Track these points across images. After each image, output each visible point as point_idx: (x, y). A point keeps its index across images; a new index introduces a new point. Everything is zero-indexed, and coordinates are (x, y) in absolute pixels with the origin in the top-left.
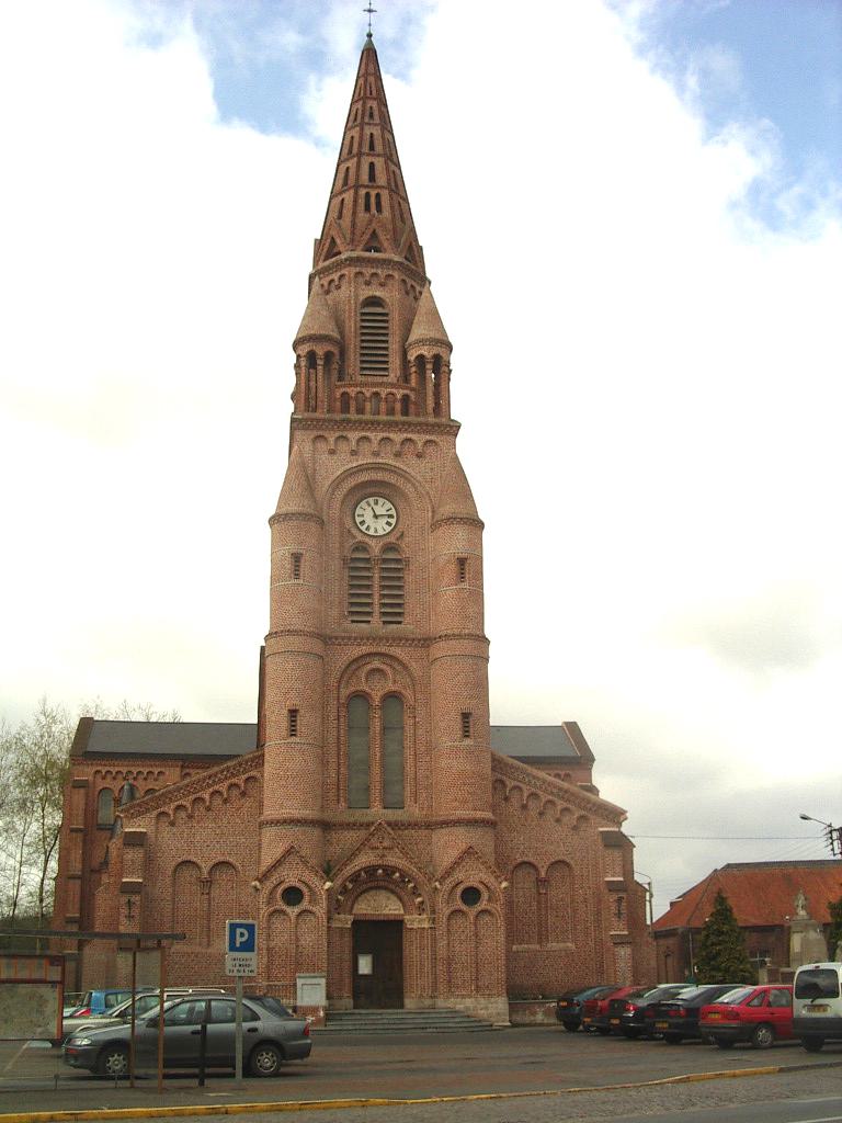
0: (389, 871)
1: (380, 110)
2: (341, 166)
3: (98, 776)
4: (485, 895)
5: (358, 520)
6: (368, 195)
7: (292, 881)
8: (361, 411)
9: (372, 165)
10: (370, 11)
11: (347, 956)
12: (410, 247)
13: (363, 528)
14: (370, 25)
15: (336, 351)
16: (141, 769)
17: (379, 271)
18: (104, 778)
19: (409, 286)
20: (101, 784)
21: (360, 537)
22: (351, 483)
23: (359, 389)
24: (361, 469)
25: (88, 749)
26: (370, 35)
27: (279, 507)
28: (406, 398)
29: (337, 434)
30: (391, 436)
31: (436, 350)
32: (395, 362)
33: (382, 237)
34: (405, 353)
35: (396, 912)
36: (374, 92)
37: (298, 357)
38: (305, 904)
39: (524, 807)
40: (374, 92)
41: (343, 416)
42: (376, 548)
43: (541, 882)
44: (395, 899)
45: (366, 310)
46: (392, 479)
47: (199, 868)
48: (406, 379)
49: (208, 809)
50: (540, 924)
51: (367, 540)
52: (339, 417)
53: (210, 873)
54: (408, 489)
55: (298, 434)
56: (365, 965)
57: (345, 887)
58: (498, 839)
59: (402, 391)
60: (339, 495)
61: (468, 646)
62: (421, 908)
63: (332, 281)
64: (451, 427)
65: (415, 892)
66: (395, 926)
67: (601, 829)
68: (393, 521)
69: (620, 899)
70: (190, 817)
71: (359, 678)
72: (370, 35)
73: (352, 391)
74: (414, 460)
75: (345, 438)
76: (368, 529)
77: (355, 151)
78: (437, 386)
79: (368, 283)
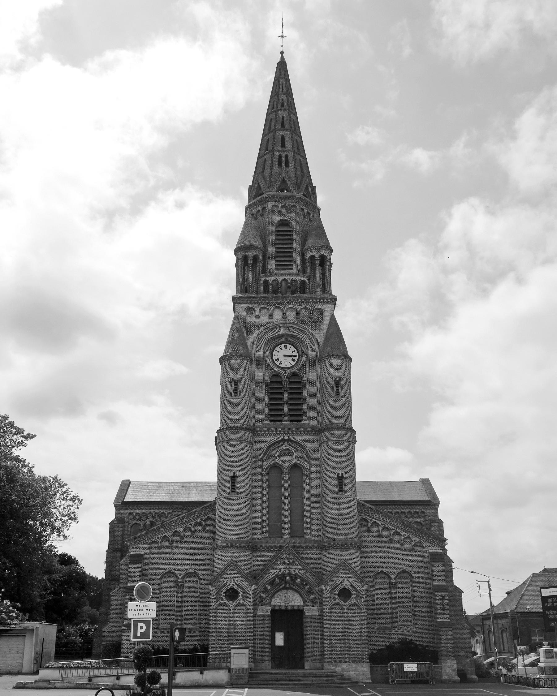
0: (294, 577)
1: (288, 100)
2: (264, 138)
4: (354, 594)
5: (275, 358)
6: (280, 156)
7: (232, 585)
8: (275, 291)
9: (283, 138)
10: (282, 37)
11: (267, 633)
12: (307, 188)
13: (278, 363)
14: (282, 46)
15: (260, 255)
16: (158, 512)
17: (287, 204)
18: (134, 517)
19: (306, 212)
20: (132, 521)
21: (275, 369)
22: (270, 335)
23: (274, 278)
24: (276, 326)
25: (126, 499)
26: (282, 53)
27: (225, 352)
28: (303, 283)
29: (261, 306)
30: (295, 306)
31: (322, 252)
32: (297, 260)
33: (288, 183)
34: (303, 255)
35: (299, 604)
36: (285, 90)
37: (238, 259)
38: (239, 600)
39: (380, 536)
40: (285, 90)
41: (264, 295)
42: (285, 375)
43: (392, 586)
44: (298, 595)
45: (281, 229)
46: (295, 333)
47: (176, 576)
48: (304, 272)
49: (182, 538)
50: (392, 613)
51: (280, 370)
52: (261, 295)
53: (183, 579)
54: (305, 339)
55: (238, 306)
56: (279, 639)
57: (266, 588)
58: (363, 556)
59: (300, 278)
60: (263, 343)
61: (344, 434)
62: (314, 603)
63: (259, 211)
64: (331, 299)
65: (310, 592)
66: (299, 613)
67: (430, 551)
68: (296, 358)
69: (443, 598)
70: (171, 543)
71: (275, 456)
72: (282, 53)
73: (270, 280)
74: (308, 321)
75: (265, 308)
77: (272, 128)
78: (323, 274)
79: (280, 212)
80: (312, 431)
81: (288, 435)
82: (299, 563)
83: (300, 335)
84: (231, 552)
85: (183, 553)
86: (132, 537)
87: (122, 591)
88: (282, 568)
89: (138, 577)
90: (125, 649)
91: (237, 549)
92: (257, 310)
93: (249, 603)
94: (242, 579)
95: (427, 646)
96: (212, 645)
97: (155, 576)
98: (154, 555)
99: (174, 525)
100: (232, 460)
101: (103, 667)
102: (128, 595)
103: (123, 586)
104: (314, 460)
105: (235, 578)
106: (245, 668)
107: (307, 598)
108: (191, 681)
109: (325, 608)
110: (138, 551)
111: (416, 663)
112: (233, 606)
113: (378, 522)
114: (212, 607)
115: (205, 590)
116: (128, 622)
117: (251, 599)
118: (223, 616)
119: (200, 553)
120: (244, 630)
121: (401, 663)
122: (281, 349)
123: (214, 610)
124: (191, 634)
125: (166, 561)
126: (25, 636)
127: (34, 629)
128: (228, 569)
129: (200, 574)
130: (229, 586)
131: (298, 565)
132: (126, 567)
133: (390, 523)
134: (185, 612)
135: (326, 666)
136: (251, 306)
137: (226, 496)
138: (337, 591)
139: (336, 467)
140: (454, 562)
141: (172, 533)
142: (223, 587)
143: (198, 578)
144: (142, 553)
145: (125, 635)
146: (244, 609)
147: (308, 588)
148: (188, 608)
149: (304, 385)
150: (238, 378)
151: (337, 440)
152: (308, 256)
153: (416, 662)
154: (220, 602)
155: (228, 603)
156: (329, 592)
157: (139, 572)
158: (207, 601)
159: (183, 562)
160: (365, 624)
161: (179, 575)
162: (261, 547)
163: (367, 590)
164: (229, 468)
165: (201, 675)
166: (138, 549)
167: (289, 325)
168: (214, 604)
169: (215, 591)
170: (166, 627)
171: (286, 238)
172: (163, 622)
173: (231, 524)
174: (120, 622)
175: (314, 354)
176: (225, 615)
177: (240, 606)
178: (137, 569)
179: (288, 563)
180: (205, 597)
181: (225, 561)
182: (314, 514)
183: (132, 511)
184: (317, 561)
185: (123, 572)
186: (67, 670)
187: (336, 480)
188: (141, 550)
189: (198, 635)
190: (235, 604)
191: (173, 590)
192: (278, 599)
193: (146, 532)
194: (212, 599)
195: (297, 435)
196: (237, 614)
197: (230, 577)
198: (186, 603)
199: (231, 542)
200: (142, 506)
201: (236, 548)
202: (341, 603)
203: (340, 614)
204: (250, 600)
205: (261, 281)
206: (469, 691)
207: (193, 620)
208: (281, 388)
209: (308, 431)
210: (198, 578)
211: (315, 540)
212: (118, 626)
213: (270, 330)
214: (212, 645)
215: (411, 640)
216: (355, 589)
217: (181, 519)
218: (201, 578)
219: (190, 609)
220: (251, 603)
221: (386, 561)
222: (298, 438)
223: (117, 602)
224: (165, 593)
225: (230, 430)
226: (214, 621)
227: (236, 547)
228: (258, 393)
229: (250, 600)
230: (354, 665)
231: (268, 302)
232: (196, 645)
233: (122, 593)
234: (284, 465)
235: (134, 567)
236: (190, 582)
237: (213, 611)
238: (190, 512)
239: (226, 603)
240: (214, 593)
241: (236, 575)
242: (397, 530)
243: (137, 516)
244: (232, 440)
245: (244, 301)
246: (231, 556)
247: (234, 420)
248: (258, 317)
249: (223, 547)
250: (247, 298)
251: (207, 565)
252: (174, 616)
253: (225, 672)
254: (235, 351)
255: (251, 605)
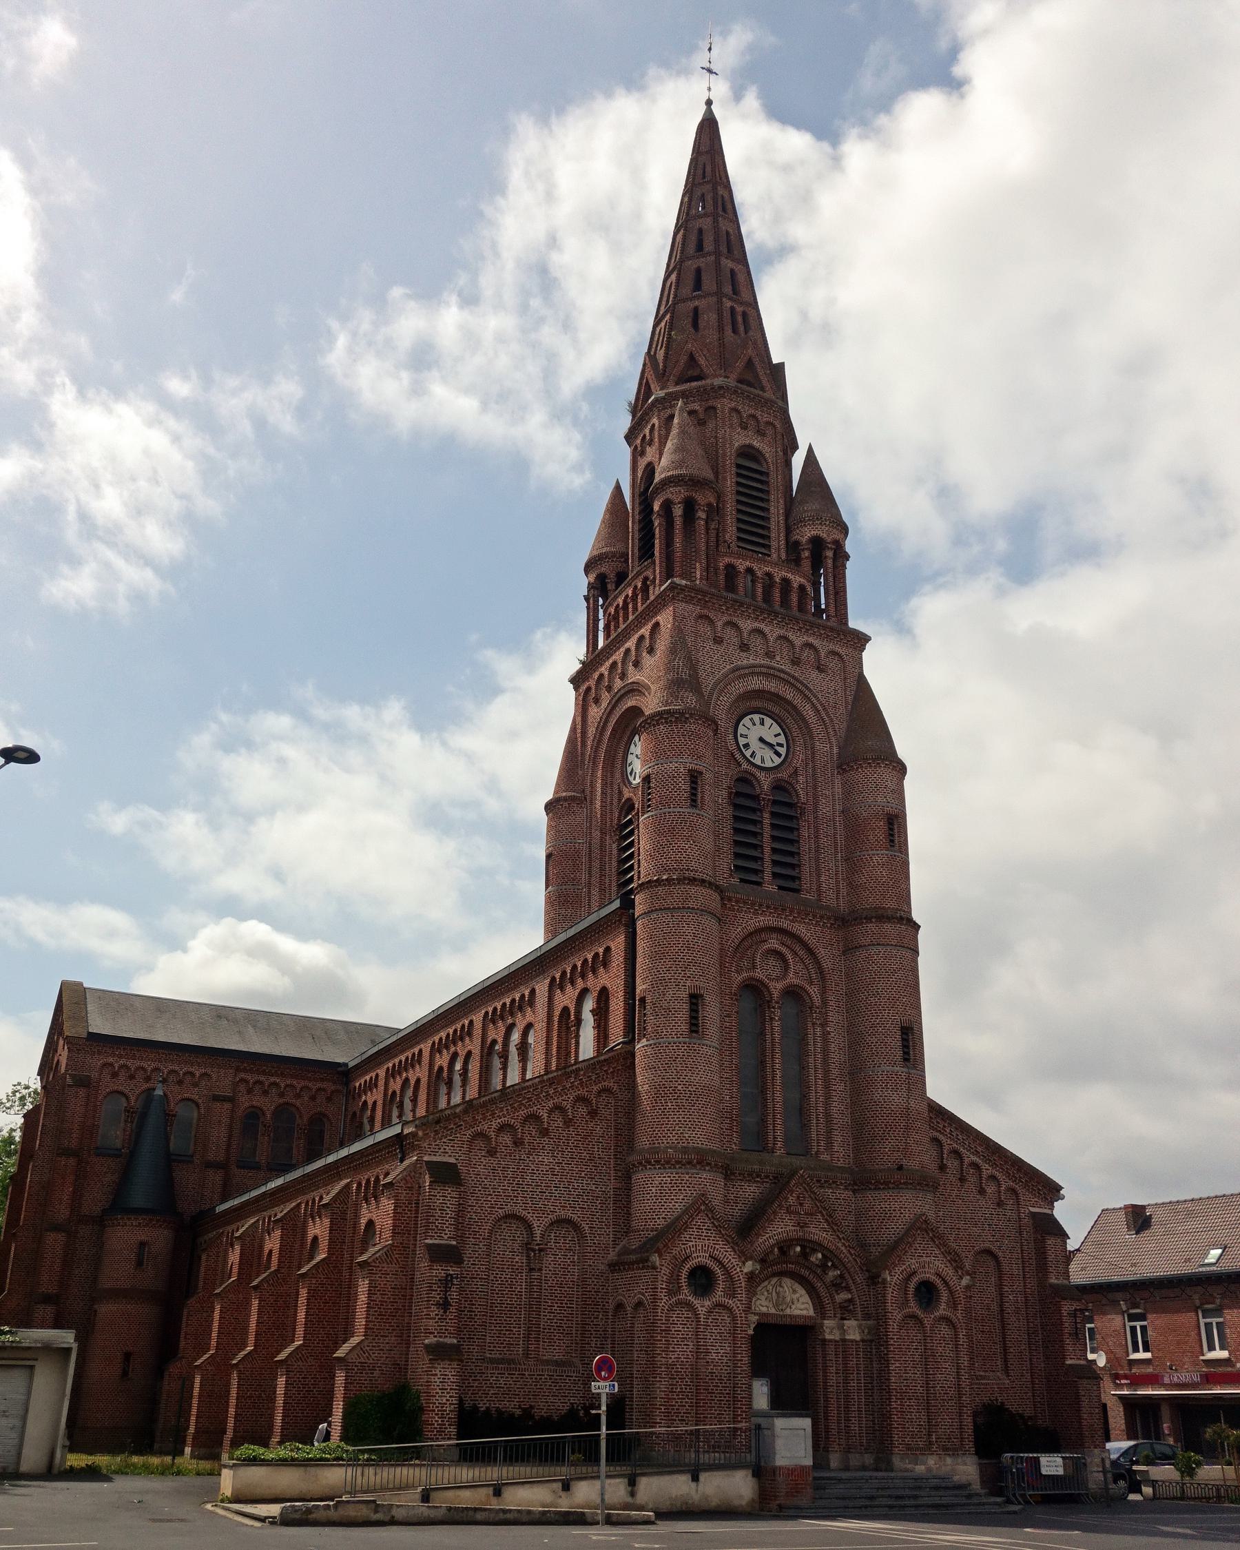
3: (106, 1071)
5: (742, 741)
7: (701, 1258)
10: (710, 71)
13: (748, 754)
18: (115, 1075)
21: (745, 766)
24: (753, 671)
35: (804, 1313)
42: (766, 782)
46: (789, 694)
47: (529, 1227)
49: (545, 1132)
51: (754, 770)
53: (543, 1236)
61: (909, 954)
70: (518, 1143)
72: (709, 103)
74: (814, 674)
76: (753, 754)
80: (829, 918)
81: (782, 918)
82: (823, 1215)
83: (798, 701)
84: (696, 1178)
85: (545, 1170)
86: (431, 1117)
87: (397, 1256)
88: (791, 1224)
89: (452, 1223)
90: (436, 1412)
91: (709, 1170)
92: (719, 624)
93: (739, 1305)
94: (723, 1245)
95: (1030, 1418)
96: (660, 1405)
97: (480, 1224)
98: (476, 1170)
99: (528, 1098)
100: (694, 957)
101: (368, 1460)
102: (435, 1268)
103: (401, 1243)
104: (833, 984)
105: (708, 1240)
106: (806, 1466)
107: (828, 1300)
108: (670, 1498)
109: (890, 1325)
110: (442, 1154)
111: (1060, 1455)
112: (704, 1309)
113: (941, 1137)
114: (659, 1311)
115: (596, 1268)
116: (436, 1339)
117: (742, 1294)
118: (682, 1334)
119: (583, 1175)
120: (726, 1370)
121: (1035, 1455)
122: (754, 724)
123: (664, 1318)
124: (563, 1376)
125: (506, 1188)
126: (32, 1367)
127: (72, 1348)
128: (694, 1218)
129: (583, 1225)
130: (697, 1261)
131: (821, 1220)
132: (408, 1194)
133: (963, 1142)
134: (546, 1320)
135: (897, 1462)
136: (705, 612)
137: (681, 1039)
138: (912, 1285)
139: (898, 1004)
140: (1069, 1238)
141: (522, 1116)
142: (683, 1262)
143: (575, 1236)
144: (452, 1160)
145: (436, 1375)
146: (726, 1318)
147: (834, 1276)
148: (553, 1311)
149: (800, 814)
150: (701, 767)
151: (898, 944)
152: (806, 537)
153: (1059, 1452)
154: (677, 1298)
155: (695, 1302)
156: (897, 1287)
157: (453, 1209)
158: (600, 1294)
159: (545, 1193)
160: (966, 1365)
161: (535, 1225)
162: (738, 1172)
163: (968, 1287)
164: (686, 974)
165: (693, 1485)
166: (442, 1150)
167: (778, 674)
168: (664, 1301)
169: (666, 1269)
170: (501, 1356)
171: (755, 484)
172: (493, 1343)
173: (693, 1108)
174: (393, 1338)
175: (827, 749)
176: (684, 1331)
177: (717, 1310)
178: (448, 1203)
179: (803, 1213)
180: (595, 1283)
181: (681, 1198)
182: (836, 1107)
183: (111, 1060)
184: (846, 1214)
185: (401, 1207)
186: (448, 1468)
187: (899, 1033)
188: (450, 1154)
189: (579, 1380)
190: (708, 1306)
191: (517, 1262)
192: (763, 1298)
193: (466, 1107)
194: (659, 1290)
195: (800, 921)
196: (712, 1329)
197: (699, 1239)
198: (547, 1296)
199: (697, 1151)
200: (138, 1051)
201: (707, 1168)
202: (919, 1313)
203: (916, 1339)
204: (741, 1297)
205: (721, 564)
206: (852, 1523)
207: (563, 1340)
208: (754, 810)
209: (822, 917)
210: (575, 1236)
211: (839, 1165)
212: (387, 1350)
213: (740, 677)
214: (660, 1405)
215: (1002, 1403)
216: (946, 1283)
217: (546, 1085)
218: (587, 1237)
219: (558, 1313)
220: (743, 1304)
221: (953, 1224)
222: (801, 929)
223: (386, 1284)
224: (499, 1268)
225: (688, 884)
226: (663, 1346)
227: (709, 1164)
228: (720, 811)
229: (741, 1297)
230: (949, 1460)
231: (740, 613)
232: (575, 1405)
233: (397, 1261)
234: (772, 985)
235: (441, 1194)
236: (558, 1245)
237: (662, 1320)
238: (567, 1070)
239: (690, 1300)
240: (664, 1274)
241: (712, 1233)
242: (974, 1158)
243: (123, 1075)
244: (693, 908)
245: (694, 597)
246: (696, 1186)
247: (693, 863)
248: (718, 641)
249: (678, 1162)
250: (701, 594)
251: (600, 1203)
252: (519, 1328)
253: (747, 1476)
254: (693, 706)
255: (743, 1311)
